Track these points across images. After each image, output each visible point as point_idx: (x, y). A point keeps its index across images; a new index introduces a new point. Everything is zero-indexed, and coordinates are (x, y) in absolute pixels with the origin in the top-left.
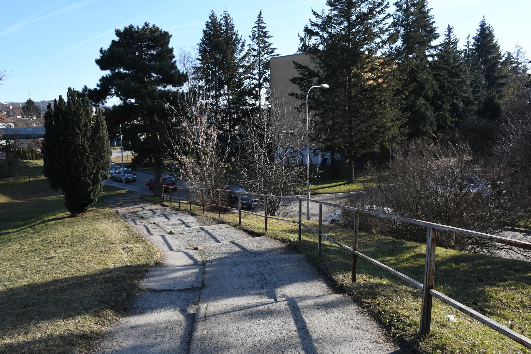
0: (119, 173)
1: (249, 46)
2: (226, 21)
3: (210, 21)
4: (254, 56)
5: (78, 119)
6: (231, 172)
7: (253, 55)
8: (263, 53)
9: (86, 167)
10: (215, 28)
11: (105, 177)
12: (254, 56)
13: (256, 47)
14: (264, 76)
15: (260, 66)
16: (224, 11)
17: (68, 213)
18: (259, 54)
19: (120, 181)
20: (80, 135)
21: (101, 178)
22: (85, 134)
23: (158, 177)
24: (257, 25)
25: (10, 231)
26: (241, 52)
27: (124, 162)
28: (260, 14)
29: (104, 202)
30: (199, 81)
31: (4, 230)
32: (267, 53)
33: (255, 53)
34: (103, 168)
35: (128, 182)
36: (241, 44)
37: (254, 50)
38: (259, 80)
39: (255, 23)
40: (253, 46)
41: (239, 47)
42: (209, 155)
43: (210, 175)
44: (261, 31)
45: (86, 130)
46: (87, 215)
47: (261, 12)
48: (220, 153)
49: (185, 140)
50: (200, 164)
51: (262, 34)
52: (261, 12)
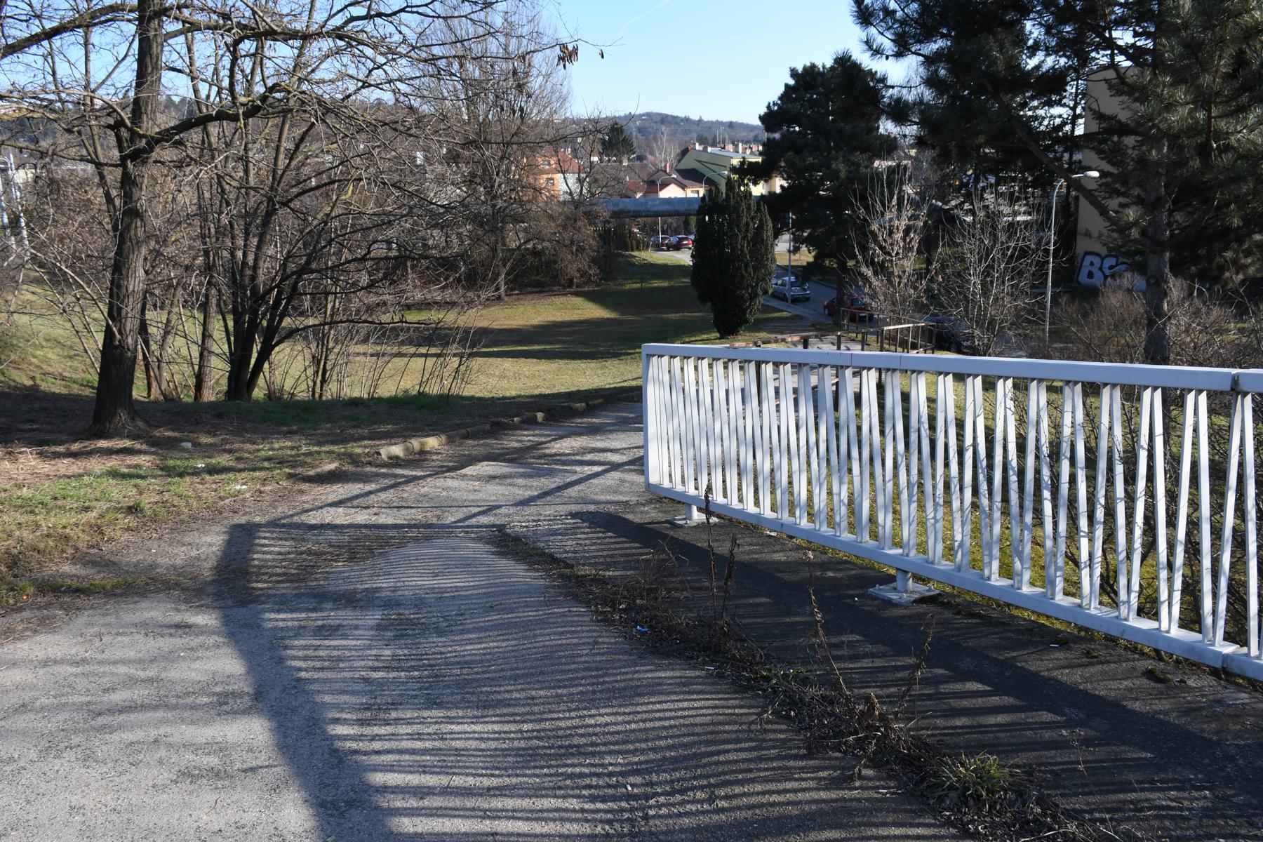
0: (783, 284)
5: (739, 216)
9: (742, 277)
11: (765, 292)
17: (718, 335)
19: (783, 298)
20: (740, 237)
21: (760, 293)
27: (793, 264)
29: (758, 326)
34: (763, 280)
35: (796, 300)
38: (1074, 109)
45: (747, 231)
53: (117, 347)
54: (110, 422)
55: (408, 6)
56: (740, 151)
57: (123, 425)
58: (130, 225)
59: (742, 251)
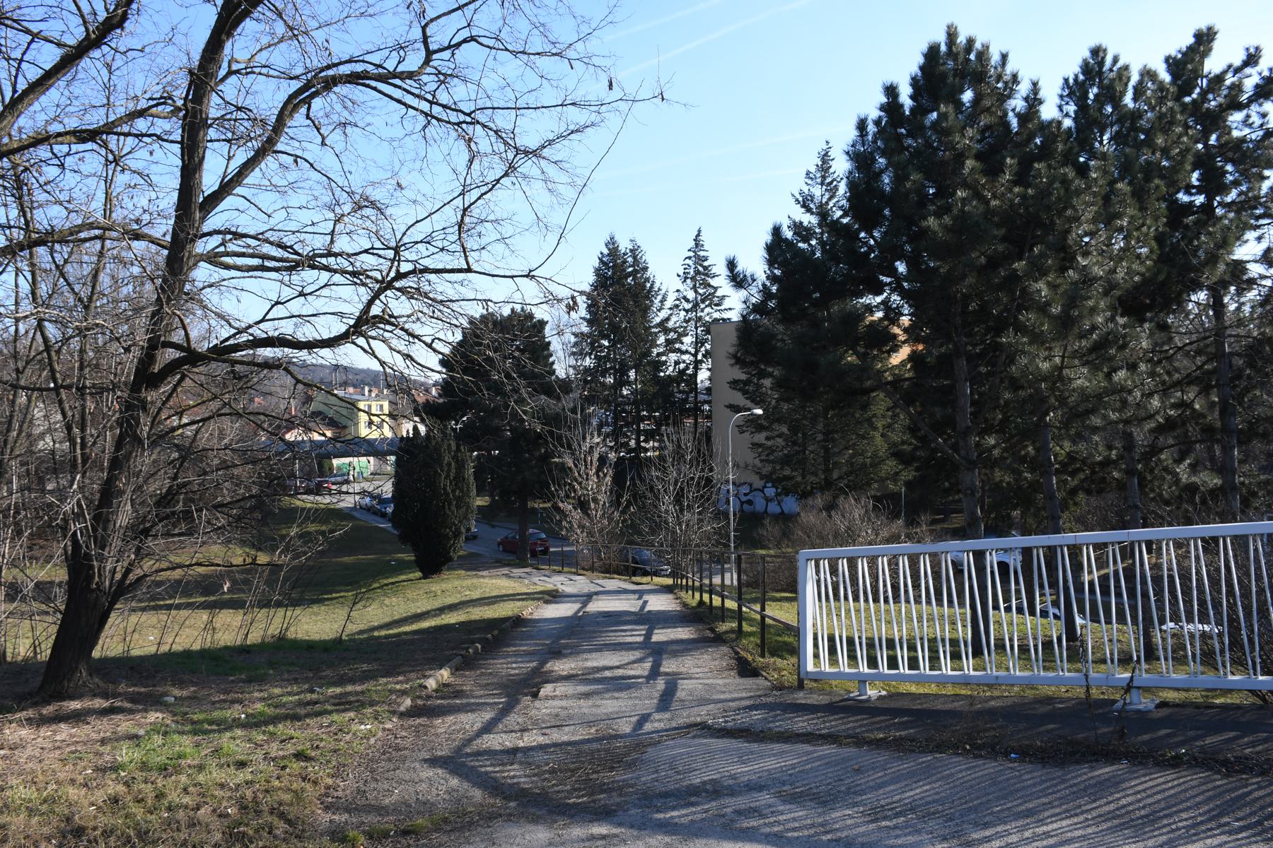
1: (676, 294)
2: (635, 258)
3: (606, 251)
4: (687, 311)
6: (627, 527)
7: (684, 310)
8: (702, 306)
10: (614, 261)
12: (687, 311)
13: (691, 295)
14: (703, 349)
15: (696, 328)
16: (631, 241)
17: (419, 574)
18: (696, 305)
22: (447, 476)
23: (522, 532)
24: (692, 254)
25: (334, 595)
26: (659, 311)
28: (698, 235)
30: (583, 359)
31: (327, 594)
32: (710, 305)
33: (688, 306)
36: (659, 298)
37: (687, 300)
38: (695, 355)
39: (689, 250)
40: (685, 294)
41: (657, 302)
42: (601, 503)
43: (601, 531)
44: (701, 265)
46: (444, 576)
47: (699, 231)
48: (616, 503)
49: (570, 484)
50: (588, 515)
51: (701, 269)
52: (699, 231)
53: (93, 590)
54: (69, 680)
55: (372, 248)
56: (367, 393)
57: (84, 682)
58: (131, 453)
59: (445, 489)
